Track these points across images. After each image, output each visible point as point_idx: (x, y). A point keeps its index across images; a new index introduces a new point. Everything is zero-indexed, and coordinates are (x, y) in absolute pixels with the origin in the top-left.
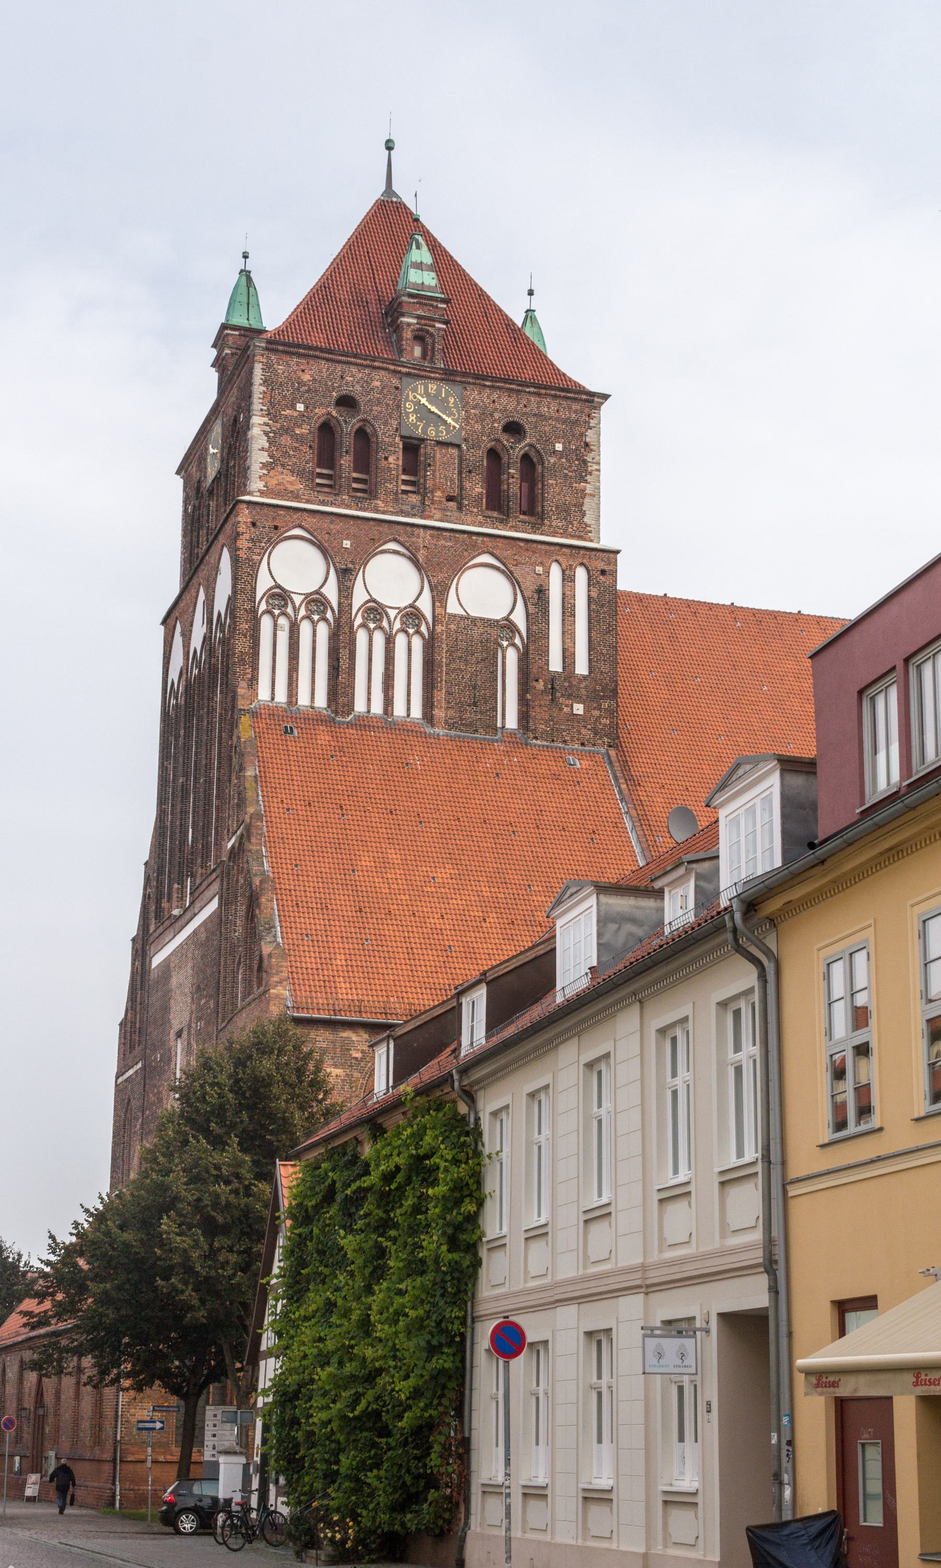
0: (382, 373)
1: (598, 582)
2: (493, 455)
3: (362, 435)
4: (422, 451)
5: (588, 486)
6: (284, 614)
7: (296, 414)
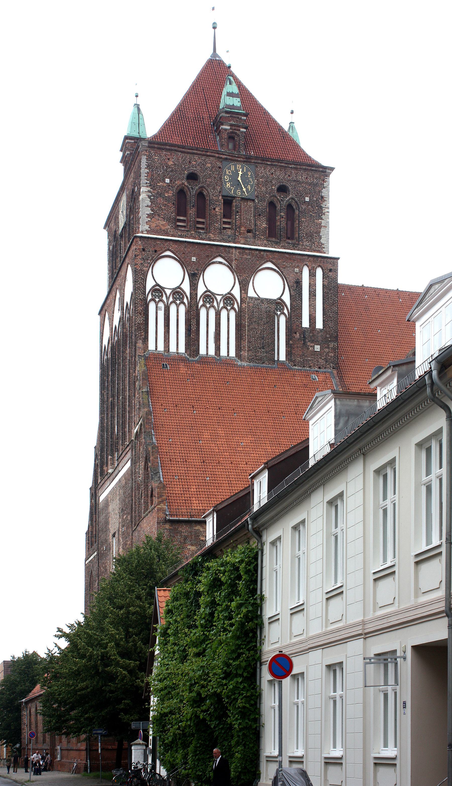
0: (212, 158)
1: (328, 276)
2: (272, 205)
3: (201, 195)
4: (234, 204)
5: (323, 221)
6: (161, 300)
7: (165, 185)
